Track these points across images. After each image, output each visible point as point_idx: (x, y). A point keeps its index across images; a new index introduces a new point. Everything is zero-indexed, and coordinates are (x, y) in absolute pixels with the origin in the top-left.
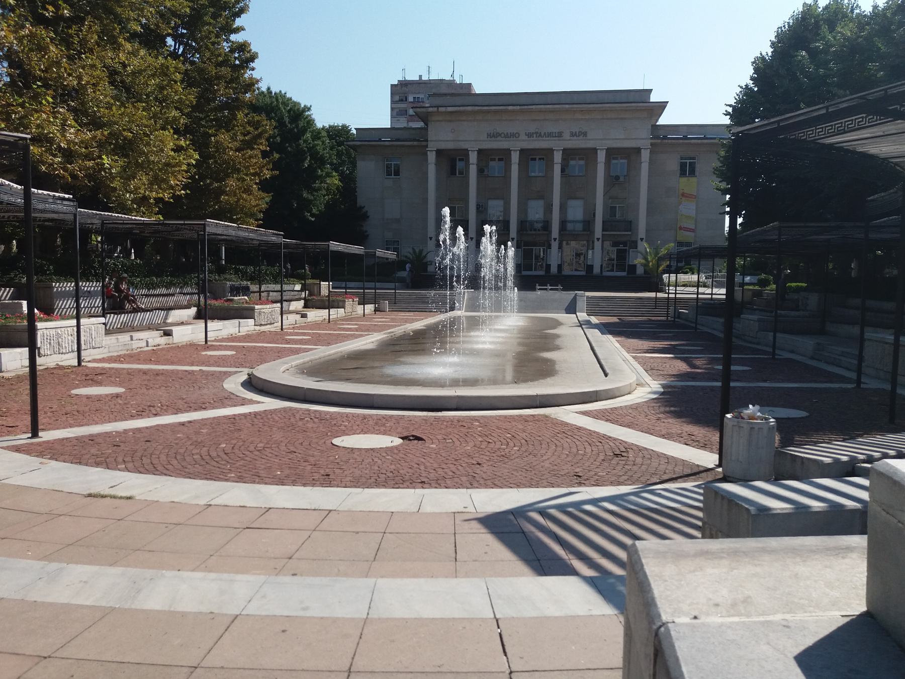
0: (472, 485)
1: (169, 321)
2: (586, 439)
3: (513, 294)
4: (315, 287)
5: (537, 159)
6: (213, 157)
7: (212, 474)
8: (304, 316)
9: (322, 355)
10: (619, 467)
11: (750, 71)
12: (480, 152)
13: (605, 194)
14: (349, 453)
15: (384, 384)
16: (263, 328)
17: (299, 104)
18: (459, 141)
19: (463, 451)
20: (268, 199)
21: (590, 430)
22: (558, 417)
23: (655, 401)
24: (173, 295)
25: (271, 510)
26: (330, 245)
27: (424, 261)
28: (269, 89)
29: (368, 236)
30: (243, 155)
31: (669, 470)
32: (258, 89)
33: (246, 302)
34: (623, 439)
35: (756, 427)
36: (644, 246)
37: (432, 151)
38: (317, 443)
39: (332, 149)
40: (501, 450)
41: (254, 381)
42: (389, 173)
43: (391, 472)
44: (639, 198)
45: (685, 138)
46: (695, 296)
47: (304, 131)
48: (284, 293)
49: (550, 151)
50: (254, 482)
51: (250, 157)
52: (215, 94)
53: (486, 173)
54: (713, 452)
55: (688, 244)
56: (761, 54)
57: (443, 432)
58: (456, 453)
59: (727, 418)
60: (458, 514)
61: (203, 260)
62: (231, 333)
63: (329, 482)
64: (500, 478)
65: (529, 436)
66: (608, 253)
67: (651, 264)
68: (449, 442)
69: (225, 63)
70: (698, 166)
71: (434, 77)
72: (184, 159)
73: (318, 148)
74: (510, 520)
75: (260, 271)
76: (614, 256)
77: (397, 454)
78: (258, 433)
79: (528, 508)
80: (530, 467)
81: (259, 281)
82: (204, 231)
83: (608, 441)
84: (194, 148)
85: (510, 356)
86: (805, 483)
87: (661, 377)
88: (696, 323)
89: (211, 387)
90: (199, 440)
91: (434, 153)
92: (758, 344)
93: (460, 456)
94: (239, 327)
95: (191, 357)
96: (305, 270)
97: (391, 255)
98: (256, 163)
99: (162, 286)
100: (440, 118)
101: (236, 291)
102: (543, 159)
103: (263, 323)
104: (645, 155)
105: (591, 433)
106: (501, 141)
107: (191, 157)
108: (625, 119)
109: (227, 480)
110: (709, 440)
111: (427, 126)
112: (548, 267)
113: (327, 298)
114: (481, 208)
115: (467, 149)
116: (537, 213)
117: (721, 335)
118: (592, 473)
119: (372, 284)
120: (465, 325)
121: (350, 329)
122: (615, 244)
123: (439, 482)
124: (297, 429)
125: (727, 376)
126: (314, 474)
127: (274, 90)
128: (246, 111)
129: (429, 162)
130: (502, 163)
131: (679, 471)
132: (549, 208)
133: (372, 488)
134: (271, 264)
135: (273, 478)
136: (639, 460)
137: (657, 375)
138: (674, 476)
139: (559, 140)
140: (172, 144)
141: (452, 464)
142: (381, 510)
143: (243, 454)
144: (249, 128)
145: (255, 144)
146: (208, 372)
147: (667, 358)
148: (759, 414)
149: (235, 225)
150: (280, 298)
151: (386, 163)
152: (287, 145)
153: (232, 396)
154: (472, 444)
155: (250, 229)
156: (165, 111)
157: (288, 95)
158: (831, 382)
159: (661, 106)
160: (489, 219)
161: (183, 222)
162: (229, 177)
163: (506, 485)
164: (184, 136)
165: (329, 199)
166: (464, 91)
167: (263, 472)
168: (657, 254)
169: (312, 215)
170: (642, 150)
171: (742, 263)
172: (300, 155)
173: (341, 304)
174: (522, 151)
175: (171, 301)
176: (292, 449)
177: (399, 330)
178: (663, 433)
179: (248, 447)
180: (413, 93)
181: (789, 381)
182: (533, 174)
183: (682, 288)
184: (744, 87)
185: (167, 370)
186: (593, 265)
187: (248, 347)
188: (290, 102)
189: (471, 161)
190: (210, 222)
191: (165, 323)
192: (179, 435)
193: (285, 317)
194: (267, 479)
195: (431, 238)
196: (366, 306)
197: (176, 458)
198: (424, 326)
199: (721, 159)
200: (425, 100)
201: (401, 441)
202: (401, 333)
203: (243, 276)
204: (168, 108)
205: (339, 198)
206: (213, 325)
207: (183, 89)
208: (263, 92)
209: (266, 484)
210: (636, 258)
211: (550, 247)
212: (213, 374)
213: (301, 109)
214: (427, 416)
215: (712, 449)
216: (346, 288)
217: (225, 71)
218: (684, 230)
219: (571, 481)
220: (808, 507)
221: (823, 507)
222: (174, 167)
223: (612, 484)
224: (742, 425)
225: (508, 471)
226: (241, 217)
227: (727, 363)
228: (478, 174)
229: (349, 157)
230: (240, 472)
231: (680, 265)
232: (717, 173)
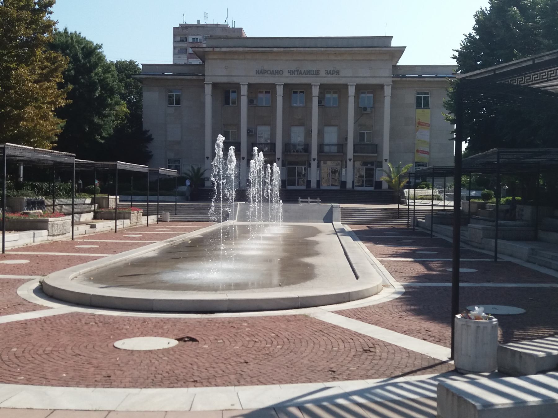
2: (340, 336)
3: (279, 206)
5: (298, 92)
8: (93, 227)
9: (108, 263)
10: (367, 362)
11: (473, 23)
12: (250, 86)
17: (92, 43)
18: (231, 76)
19: (232, 350)
20: (62, 124)
21: (343, 328)
22: (317, 316)
23: (398, 300)
26: (117, 164)
27: (202, 177)
28: (66, 29)
29: (152, 155)
30: (40, 87)
32: (55, 30)
33: (41, 215)
34: (371, 336)
35: (482, 326)
36: (388, 166)
40: (266, 349)
41: (45, 288)
42: (171, 103)
45: (420, 76)
46: (430, 208)
47: (96, 65)
48: (75, 206)
50: (41, 384)
51: (47, 88)
52: (16, 34)
53: (255, 103)
55: (424, 164)
56: (481, 9)
57: (215, 332)
58: (226, 352)
59: (457, 318)
60: (226, 411)
63: (110, 383)
66: (358, 171)
67: (394, 181)
68: (221, 343)
70: (431, 100)
71: (210, 22)
73: (108, 80)
74: (272, 415)
75: (54, 187)
76: (363, 173)
77: (173, 355)
79: (289, 404)
80: (291, 364)
82: (4, 153)
83: (358, 338)
87: (403, 279)
88: (432, 231)
89: (5, 293)
92: (483, 249)
93: (230, 356)
96: (94, 184)
97: (172, 172)
98: (52, 93)
100: (215, 57)
101: (32, 205)
102: (303, 92)
103: (56, 234)
104: (388, 91)
105: (344, 331)
106: (268, 77)
108: (371, 60)
109: (17, 383)
110: (443, 335)
112: (309, 182)
114: (251, 133)
118: (345, 368)
119: (155, 198)
122: (365, 164)
123: (210, 380)
124: (82, 333)
125: (456, 278)
126: (97, 376)
128: (44, 49)
129: (206, 93)
130: (269, 95)
131: (419, 364)
132: (308, 133)
134: (65, 180)
135: (59, 380)
136: (384, 355)
137: (400, 277)
138: (414, 369)
139: (316, 77)
141: (222, 363)
142: (156, 410)
144: (46, 63)
147: (408, 261)
152: (80, 77)
153: (25, 302)
154: (240, 344)
155: (45, 151)
158: (544, 282)
162: (28, 105)
163: (269, 382)
165: (118, 124)
166: (234, 35)
167: (49, 374)
168: (398, 172)
169: (102, 138)
171: (468, 179)
172: (92, 86)
173: (127, 215)
174: (286, 86)
176: (77, 351)
177: (178, 239)
179: (37, 350)
181: (508, 281)
182: (295, 105)
183: (420, 201)
184: (468, 35)
186: (346, 181)
187: (41, 256)
188: (83, 41)
189: (242, 94)
190: (9, 145)
193: (75, 227)
194: (54, 381)
198: (201, 235)
199: (450, 94)
200: (202, 41)
202: (180, 241)
203: (38, 192)
208: (60, 33)
209: (52, 385)
210: (382, 175)
211: (310, 165)
212: (8, 281)
214: (201, 318)
215: (445, 343)
216: (132, 201)
217: (26, 14)
218: (421, 153)
219: (326, 376)
220: (524, 402)
221: (537, 401)
223: (362, 377)
225: (271, 368)
227: (456, 265)
228: (248, 104)
229: (136, 87)
231: (417, 181)
232: (447, 106)
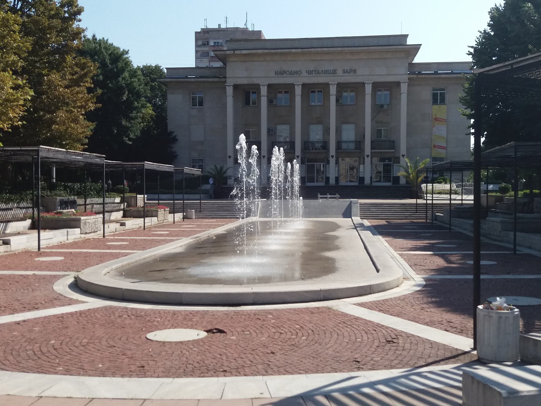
0: (267, 372)
1: (8, 231)
3: (300, 202)
4: (133, 200)
5: (316, 92)
7: (43, 368)
8: (123, 224)
9: (138, 258)
10: (391, 353)
12: (270, 86)
15: (191, 283)
16: (88, 236)
17: (119, 48)
20: (92, 127)
21: (366, 320)
22: (339, 309)
24: (11, 209)
25: (93, 400)
26: (145, 164)
28: (94, 36)
29: (177, 155)
30: (71, 91)
31: (432, 354)
32: (84, 37)
33: (74, 214)
34: (394, 327)
36: (405, 161)
37: (230, 85)
38: (134, 338)
40: (292, 340)
41: (79, 283)
43: (198, 362)
45: (436, 73)
46: (448, 202)
47: (123, 70)
49: (327, 85)
50: (79, 374)
51: (78, 93)
52: (47, 41)
55: (441, 159)
56: (496, 5)
57: (242, 324)
58: (253, 343)
59: (479, 309)
60: (256, 400)
61: (37, 179)
62: (60, 241)
63: (144, 373)
64: (291, 366)
65: (315, 326)
67: (411, 176)
68: (247, 334)
69: (56, 16)
71: (230, 25)
72: (21, 95)
73: (135, 84)
76: (381, 169)
77: (202, 346)
79: (316, 393)
80: (317, 355)
81: (85, 195)
82: (38, 155)
83: (381, 329)
84: (30, 86)
87: (423, 272)
88: (450, 225)
89: (42, 289)
90: (32, 338)
92: (502, 241)
93: (256, 346)
94: (67, 235)
95: (26, 262)
96: (124, 184)
97: (196, 171)
98: (82, 97)
99: (2, 202)
100: (236, 59)
101: (65, 204)
102: (321, 91)
103: (88, 232)
104: (404, 88)
105: (367, 322)
106: (286, 77)
107: (27, 94)
108: (387, 58)
109: (56, 373)
110: (465, 326)
112: (328, 179)
113: (143, 209)
114: (271, 132)
115: (259, 84)
116: (317, 134)
117: (472, 235)
119: (180, 196)
120: (259, 228)
122: (382, 160)
123: (239, 370)
124: (116, 325)
125: (477, 270)
128: (74, 55)
130: (287, 95)
131: (441, 354)
132: (327, 131)
133: (181, 377)
134: (95, 181)
135: (95, 370)
136: (407, 346)
137: (420, 270)
138: (437, 359)
139: (333, 76)
140: (11, 83)
141: (250, 353)
142: (189, 398)
144: (76, 69)
146: (40, 276)
147: (427, 255)
148: (505, 305)
149: (64, 150)
150: (102, 209)
151: (192, 96)
152: (109, 82)
153: (61, 297)
154: (266, 335)
155: (77, 153)
156: (6, 56)
157: (110, 42)
159: (416, 48)
161: (19, 149)
162: (59, 109)
165: (144, 126)
166: (254, 38)
167: (86, 365)
168: (416, 167)
169: (130, 139)
170: (402, 84)
171: (486, 173)
172: (120, 90)
173: (154, 213)
174: (304, 85)
175: (9, 214)
176: (112, 343)
177: (204, 235)
178: (427, 320)
179: (74, 342)
180: (213, 39)
182: (313, 104)
183: (438, 195)
185: (5, 275)
189: (262, 94)
190: (43, 148)
191: (4, 234)
192: (14, 333)
193: (106, 225)
194: (91, 371)
196: (175, 214)
197: (12, 354)
198: (225, 231)
199: (466, 90)
200: (223, 44)
201: (205, 334)
202: (206, 237)
203: (71, 192)
204: (8, 53)
205: (153, 125)
206: (46, 235)
208: (88, 39)
209: (90, 376)
210: (399, 171)
211: (328, 162)
212: (44, 277)
214: (228, 311)
215: (467, 334)
216: (158, 200)
217: (56, 22)
218: (438, 148)
219: (351, 366)
222: (13, 102)
223: (386, 367)
224: (492, 315)
226: (69, 143)
227: (477, 258)
228: (268, 105)
230: (67, 366)
231: (435, 176)
232: (463, 101)
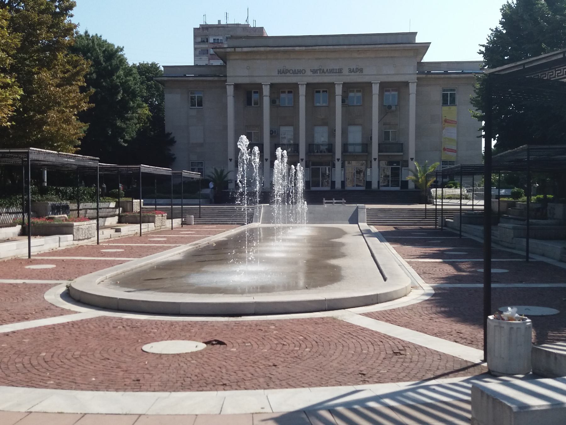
0: (269, 386)
3: (303, 206)
4: (129, 205)
5: (321, 92)
6: (36, 92)
7: (33, 382)
8: (118, 231)
9: (134, 266)
10: (398, 365)
11: (499, 17)
12: (272, 86)
13: (380, 121)
14: (157, 358)
15: (190, 293)
16: (81, 243)
17: (113, 45)
19: (260, 353)
20: (85, 128)
21: (372, 331)
22: (345, 319)
23: (428, 302)
25: (86, 416)
26: (141, 167)
28: (86, 32)
29: (175, 158)
30: (63, 90)
32: (77, 33)
33: (66, 220)
34: (401, 338)
35: (515, 327)
39: (142, 83)
40: (295, 352)
41: (72, 293)
42: (193, 105)
43: (196, 376)
44: (408, 124)
45: (446, 73)
46: (459, 207)
47: (117, 68)
48: (100, 211)
49: (333, 85)
50: (71, 389)
51: (70, 92)
52: (37, 38)
53: (277, 103)
54: (478, 348)
55: (452, 163)
56: (508, 2)
57: (242, 336)
59: (490, 319)
61: (27, 182)
63: (139, 387)
64: (293, 379)
65: (319, 338)
66: (384, 170)
67: (420, 180)
71: (231, 21)
72: (10, 95)
73: (130, 83)
74: (303, 418)
75: (78, 191)
76: (389, 173)
77: (201, 358)
78: (75, 342)
79: (319, 407)
80: (321, 367)
81: (78, 200)
82: (28, 157)
83: (388, 340)
84: (19, 84)
85: (302, 263)
86: (558, 381)
87: (432, 280)
88: (460, 231)
89: (33, 298)
90: (22, 350)
91: (232, 86)
92: (514, 249)
94: (59, 242)
96: (119, 188)
97: (195, 175)
98: (74, 97)
100: (237, 57)
101: (57, 209)
102: (326, 91)
103: (81, 238)
104: (413, 88)
106: (290, 76)
107: (16, 93)
108: (395, 57)
109: (46, 387)
111: (226, 63)
112: (333, 183)
114: (274, 134)
117: (482, 241)
118: (375, 371)
119: (179, 201)
121: (159, 242)
122: (390, 163)
123: (239, 384)
124: (111, 337)
125: (488, 278)
126: (126, 380)
127: (91, 33)
130: (291, 96)
131: (450, 366)
132: (332, 133)
133: (178, 391)
134: (88, 184)
135: (88, 384)
136: (415, 358)
137: (429, 278)
138: (446, 372)
139: (339, 76)
141: (251, 366)
142: (186, 413)
143: (62, 362)
144: (68, 67)
145: (74, 80)
146: (31, 285)
148: (517, 315)
149: (56, 152)
151: (190, 95)
153: (52, 307)
154: (268, 347)
155: (69, 155)
157: (103, 38)
159: (425, 47)
160: (280, 143)
161: (8, 151)
162: (50, 109)
163: (299, 385)
164: (10, 73)
165: (140, 127)
167: (79, 379)
168: (425, 171)
169: (125, 141)
170: (410, 84)
171: (498, 178)
172: (114, 89)
173: (151, 219)
174: (308, 85)
176: (106, 356)
177: (203, 242)
178: (436, 331)
179: (66, 355)
181: (542, 282)
182: (318, 104)
183: (447, 201)
187: (67, 260)
189: (264, 94)
190: (33, 150)
192: (3, 345)
193: (100, 232)
194: (83, 385)
195: (231, 160)
196: (173, 220)
198: (226, 237)
199: (477, 91)
200: (223, 41)
202: (205, 244)
203: (63, 197)
205: (149, 126)
206: (36, 241)
207: (9, 34)
208: (81, 36)
209: (82, 390)
210: (408, 175)
211: (334, 166)
212: (35, 286)
213: (114, 50)
214: (228, 322)
215: (478, 345)
216: (156, 205)
217: (47, 17)
218: (447, 151)
219: (357, 379)
223: (392, 380)
224: (503, 325)
227: (488, 266)
228: (271, 105)
229: (158, 89)
230: (59, 379)
231: (444, 180)
232: (474, 102)
